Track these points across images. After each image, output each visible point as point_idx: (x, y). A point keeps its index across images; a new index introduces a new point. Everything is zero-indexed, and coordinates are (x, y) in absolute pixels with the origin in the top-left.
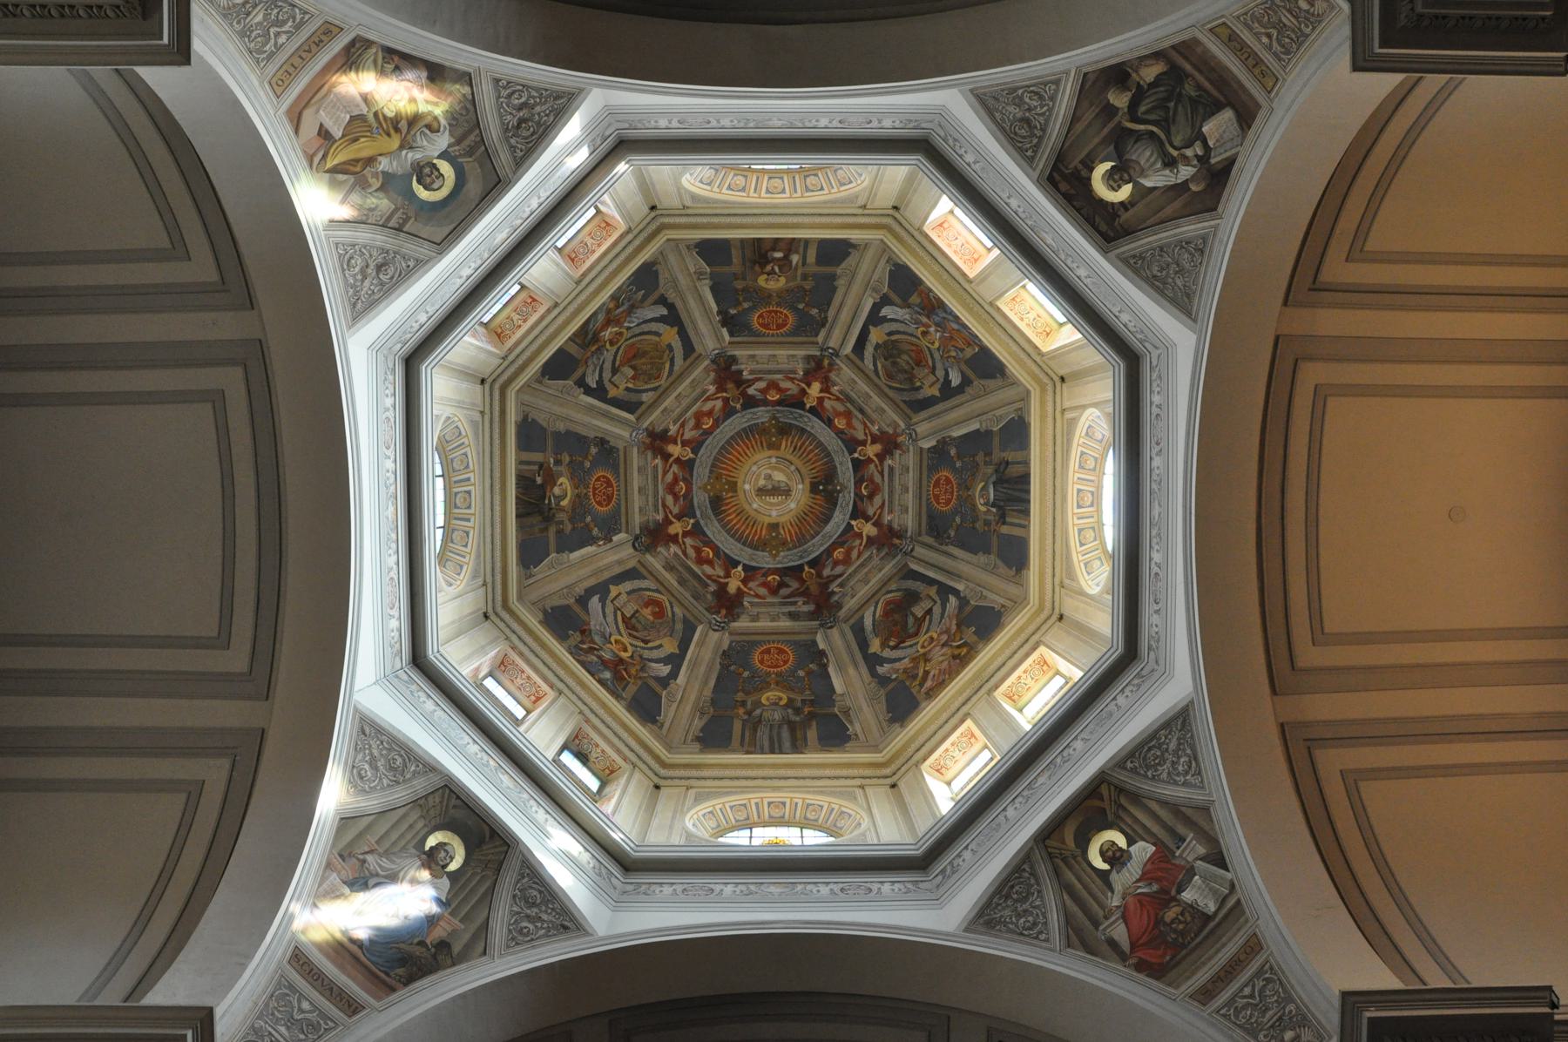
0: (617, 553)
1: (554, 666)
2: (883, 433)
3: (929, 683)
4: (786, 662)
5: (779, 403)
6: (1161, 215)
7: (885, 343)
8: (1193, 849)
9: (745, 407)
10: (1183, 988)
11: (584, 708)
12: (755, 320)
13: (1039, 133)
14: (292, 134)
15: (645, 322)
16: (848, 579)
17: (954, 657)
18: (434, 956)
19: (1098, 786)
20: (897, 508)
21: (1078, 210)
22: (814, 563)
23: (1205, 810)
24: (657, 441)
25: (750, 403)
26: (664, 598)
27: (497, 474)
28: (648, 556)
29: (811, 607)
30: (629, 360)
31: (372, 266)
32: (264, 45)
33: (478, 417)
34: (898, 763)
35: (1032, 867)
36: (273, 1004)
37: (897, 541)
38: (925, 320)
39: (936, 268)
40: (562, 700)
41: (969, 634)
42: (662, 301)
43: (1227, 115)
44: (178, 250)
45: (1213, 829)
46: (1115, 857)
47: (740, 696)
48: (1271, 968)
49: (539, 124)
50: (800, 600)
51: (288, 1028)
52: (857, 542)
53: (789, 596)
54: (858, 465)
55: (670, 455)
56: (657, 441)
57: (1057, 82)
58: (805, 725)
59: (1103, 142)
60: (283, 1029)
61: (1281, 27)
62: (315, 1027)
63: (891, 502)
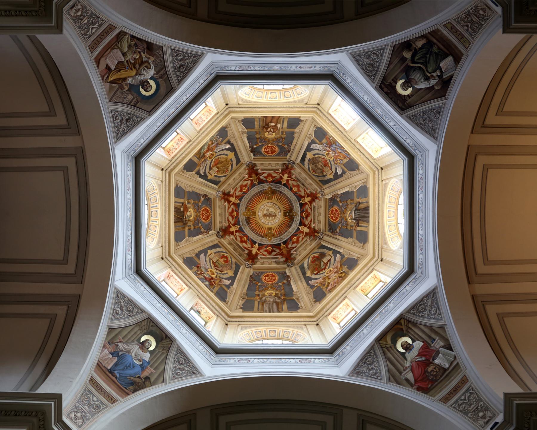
0: (211, 238)
1: (188, 278)
2: (312, 193)
3: (330, 287)
4: (274, 280)
5: (272, 182)
6: (423, 99)
7: (313, 158)
8: (438, 344)
9: (259, 183)
10: (436, 397)
11: (199, 294)
12: (263, 149)
13: (376, 69)
14: (96, 67)
15: (222, 150)
16: (298, 249)
17: (340, 277)
18: (144, 382)
19: (400, 320)
20: (317, 221)
21: (391, 99)
22: (285, 243)
23: (443, 328)
24: (226, 196)
25: (261, 182)
26: (228, 255)
27: (167, 205)
28: (222, 239)
29: (284, 259)
30: (216, 165)
31: (124, 119)
32: (88, 32)
33: (160, 183)
34: (319, 316)
35: (374, 352)
36: (83, 397)
37: (316, 234)
38: (328, 149)
39: (334, 127)
40: (191, 290)
41: (345, 268)
42: (229, 142)
43: (450, 59)
44: (52, 113)
45: (446, 335)
46: (407, 347)
47: (257, 292)
48: (472, 388)
49: (187, 67)
50: (280, 257)
51: (89, 407)
52: (301, 235)
53: (276, 255)
54: (302, 205)
55: (231, 202)
56: (226, 196)
57: (383, 49)
58: (282, 303)
59: (402, 71)
60: (86, 407)
61: (472, 22)
62: (99, 407)
63: (314, 219)
